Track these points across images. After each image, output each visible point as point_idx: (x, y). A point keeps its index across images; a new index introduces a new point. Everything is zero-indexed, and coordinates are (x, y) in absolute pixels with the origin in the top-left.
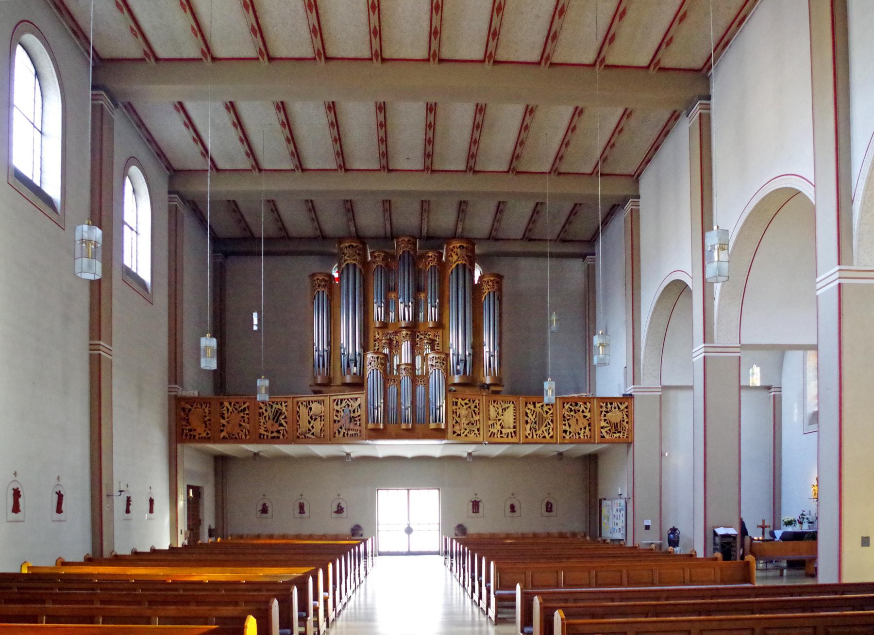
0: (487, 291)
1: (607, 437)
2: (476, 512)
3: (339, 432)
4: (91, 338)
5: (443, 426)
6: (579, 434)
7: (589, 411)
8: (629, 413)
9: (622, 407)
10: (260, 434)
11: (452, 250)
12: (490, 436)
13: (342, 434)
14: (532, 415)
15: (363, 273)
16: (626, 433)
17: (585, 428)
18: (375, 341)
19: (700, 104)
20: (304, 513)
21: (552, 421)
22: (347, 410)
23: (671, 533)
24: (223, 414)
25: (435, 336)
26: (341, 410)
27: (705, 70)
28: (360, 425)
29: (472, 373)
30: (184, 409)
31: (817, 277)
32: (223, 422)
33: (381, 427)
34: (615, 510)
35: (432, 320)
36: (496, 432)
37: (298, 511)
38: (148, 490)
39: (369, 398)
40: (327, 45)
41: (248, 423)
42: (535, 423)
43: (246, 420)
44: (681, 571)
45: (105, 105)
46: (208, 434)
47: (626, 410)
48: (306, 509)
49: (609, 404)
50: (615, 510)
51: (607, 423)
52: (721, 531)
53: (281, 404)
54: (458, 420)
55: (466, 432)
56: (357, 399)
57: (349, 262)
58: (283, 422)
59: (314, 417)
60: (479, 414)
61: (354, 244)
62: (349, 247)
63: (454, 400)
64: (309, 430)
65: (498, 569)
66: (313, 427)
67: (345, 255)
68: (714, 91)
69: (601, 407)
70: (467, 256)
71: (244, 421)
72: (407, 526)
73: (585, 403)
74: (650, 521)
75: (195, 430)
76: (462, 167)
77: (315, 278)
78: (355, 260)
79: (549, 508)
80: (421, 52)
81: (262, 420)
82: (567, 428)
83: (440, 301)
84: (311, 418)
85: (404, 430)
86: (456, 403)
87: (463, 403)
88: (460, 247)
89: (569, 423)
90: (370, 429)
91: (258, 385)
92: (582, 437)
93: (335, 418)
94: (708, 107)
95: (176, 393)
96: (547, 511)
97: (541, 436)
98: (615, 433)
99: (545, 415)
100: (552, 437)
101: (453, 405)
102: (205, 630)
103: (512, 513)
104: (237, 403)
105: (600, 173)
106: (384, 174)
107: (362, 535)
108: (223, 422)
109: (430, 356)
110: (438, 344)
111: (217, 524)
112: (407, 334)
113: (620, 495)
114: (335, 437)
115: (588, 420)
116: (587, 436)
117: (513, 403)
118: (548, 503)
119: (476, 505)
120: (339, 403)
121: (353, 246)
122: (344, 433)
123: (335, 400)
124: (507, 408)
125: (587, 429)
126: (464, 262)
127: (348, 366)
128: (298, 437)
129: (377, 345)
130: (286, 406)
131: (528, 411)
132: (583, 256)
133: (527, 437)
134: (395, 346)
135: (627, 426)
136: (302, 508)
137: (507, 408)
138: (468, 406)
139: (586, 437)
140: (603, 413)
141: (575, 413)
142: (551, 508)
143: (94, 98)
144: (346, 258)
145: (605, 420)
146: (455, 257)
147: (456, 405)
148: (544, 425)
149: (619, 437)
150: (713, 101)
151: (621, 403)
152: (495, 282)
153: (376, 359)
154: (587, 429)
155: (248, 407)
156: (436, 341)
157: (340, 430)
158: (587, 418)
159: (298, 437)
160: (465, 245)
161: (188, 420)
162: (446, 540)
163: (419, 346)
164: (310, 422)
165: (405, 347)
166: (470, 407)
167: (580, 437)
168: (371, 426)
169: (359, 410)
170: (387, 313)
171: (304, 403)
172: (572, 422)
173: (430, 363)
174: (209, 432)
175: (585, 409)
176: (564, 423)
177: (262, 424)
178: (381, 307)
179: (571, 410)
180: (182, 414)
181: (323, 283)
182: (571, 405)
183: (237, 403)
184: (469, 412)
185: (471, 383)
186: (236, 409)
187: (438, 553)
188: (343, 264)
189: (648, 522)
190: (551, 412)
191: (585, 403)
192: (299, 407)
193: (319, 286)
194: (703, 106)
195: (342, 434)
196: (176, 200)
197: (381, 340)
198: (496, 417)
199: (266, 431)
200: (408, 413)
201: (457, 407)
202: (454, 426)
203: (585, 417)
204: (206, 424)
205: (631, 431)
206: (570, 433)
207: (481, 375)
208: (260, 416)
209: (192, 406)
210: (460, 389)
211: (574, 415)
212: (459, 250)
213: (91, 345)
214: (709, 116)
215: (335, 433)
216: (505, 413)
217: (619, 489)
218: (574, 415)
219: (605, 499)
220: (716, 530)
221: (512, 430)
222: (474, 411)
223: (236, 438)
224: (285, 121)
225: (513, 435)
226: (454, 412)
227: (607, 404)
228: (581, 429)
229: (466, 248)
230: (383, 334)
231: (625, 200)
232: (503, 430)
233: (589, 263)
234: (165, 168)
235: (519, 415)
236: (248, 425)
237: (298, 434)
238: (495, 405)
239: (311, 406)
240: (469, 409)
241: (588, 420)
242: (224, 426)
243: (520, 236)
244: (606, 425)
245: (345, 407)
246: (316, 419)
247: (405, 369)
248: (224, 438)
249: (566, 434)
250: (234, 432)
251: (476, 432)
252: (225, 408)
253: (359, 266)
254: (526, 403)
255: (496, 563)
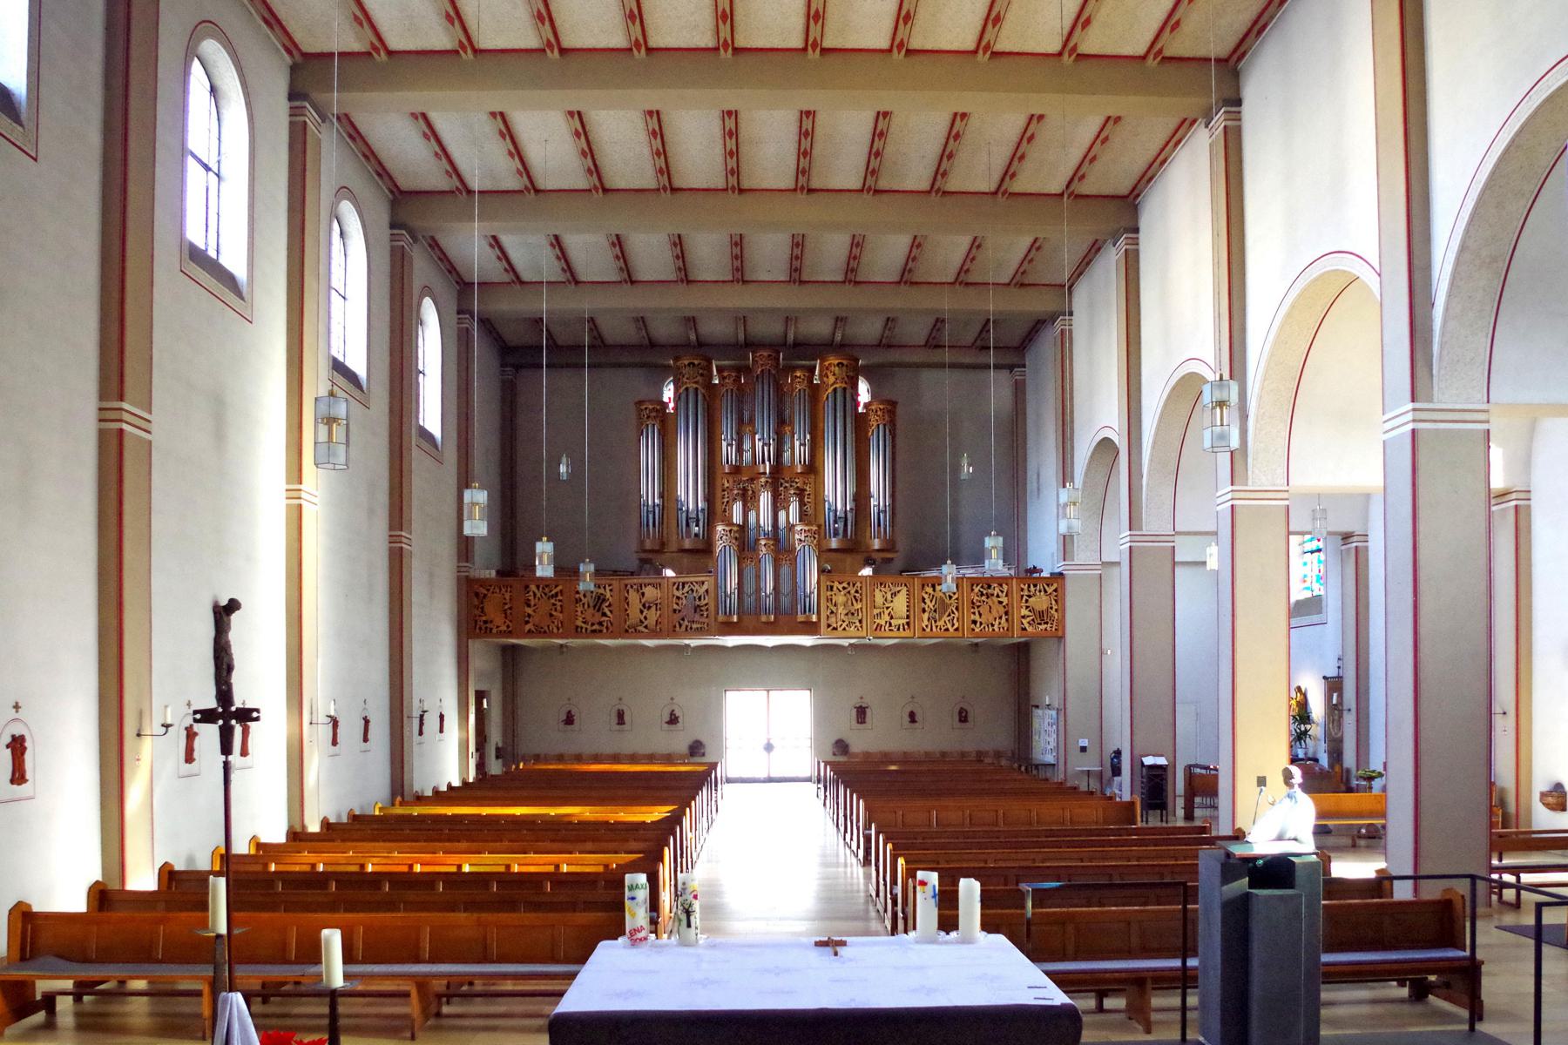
0: (875, 424)
1: (1030, 629)
2: (861, 723)
3: (680, 625)
4: (391, 529)
5: (814, 618)
6: (993, 625)
7: (1007, 596)
8: (1059, 597)
9: (1050, 590)
10: (577, 627)
11: (827, 369)
12: (876, 630)
13: (684, 627)
14: (931, 601)
15: (707, 398)
16: (1055, 623)
17: (1000, 618)
18: (724, 491)
19: (1126, 238)
20: (624, 724)
21: (957, 609)
22: (691, 596)
23: (1115, 757)
24: (529, 600)
25: (804, 483)
26: (683, 597)
27: (1132, 197)
28: (707, 617)
29: (855, 534)
30: (477, 595)
31: (1217, 491)
32: (529, 610)
33: (735, 619)
34: (1046, 724)
35: (800, 462)
36: (883, 623)
37: (616, 721)
38: (438, 703)
39: (719, 581)
40: (650, 32)
41: (561, 612)
42: (935, 611)
43: (559, 608)
44: (1061, 812)
45: (406, 246)
46: (508, 627)
47: (1055, 594)
48: (627, 718)
49: (1032, 586)
50: (1046, 724)
51: (1030, 611)
52: (1148, 761)
53: (605, 588)
54: (834, 609)
55: (844, 625)
56: (703, 583)
57: (688, 385)
58: (606, 610)
59: (647, 605)
60: (861, 600)
61: (696, 362)
62: (689, 364)
63: (828, 583)
64: (641, 622)
65: (866, 808)
66: (646, 618)
67: (683, 376)
68: (1144, 224)
69: (1022, 590)
70: (848, 376)
71: (556, 610)
72: (766, 742)
73: (1001, 585)
74: (1087, 740)
75: (491, 622)
76: (840, 278)
77: (643, 407)
78: (696, 383)
79: (963, 717)
80: (787, 182)
81: (579, 609)
82: (977, 617)
83: (811, 438)
84: (644, 606)
85: (764, 623)
86: (832, 587)
87: (840, 587)
88: (838, 364)
89: (979, 612)
90: (722, 623)
91: (581, 570)
92: (997, 629)
93: (675, 607)
94: (1136, 242)
95: (467, 574)
96: (960, 721)
97: (943, 628)
98: (1040, 624)
99: (947, 601)
100: (957, 629)
101: (827, 590)
102: (627, 860)
103: (912, 725)
104: (547, 586)
105: (1020, 282)
106: (738, 287)
107: (703, 755)
108: (529, 610)
109: (798, 528)
110: (809, 495)
111: (503, 742)
112: (767, 482)
113: (1048, 705)
114: (674, 631)
115: (1004, 607)
116: (1003, 628)
117: (906, 585)
118: (962, 711)
119: (861, 713)
120: (681, 587)
121: (694, 364)
122: (687, 626)
123: (674, 584)
124: (899, 592)
125: (1004, 618)
126: (844, 385)
127: (688, 525)
128: (627, 631)
129: (726, 496)
130: (611, 590)
131: (926, 596)
132: (1011, 367)
133: (924, 630)
134: (751, 498)
135: (1056, 615)
136: (621, 717)
137: (899, 592)
138: (846, 591)
139: (1001, 630)
140: (1025, 597)
141: (987, 598)
142: (966, 717)
143: (393, 238)
144: (685, 380)
145: (1027, 607)
146: (832, 379)
147: (832, 590)
148: (947, 614)
149: (1046, 630)
150: (1142, 235)
151: (1048, 585)
152: (885, 411)
153: (728, 533)
154: (1004, 618)
155: (561, 591)
156: (806, 490)
157: (682, 622)
158: (1004, 604)
159: (627, 631)
160: (845, 362)
161: (482, 608)
162: (819, 763)
163: (782, 497)
164: (642, 612)
165: (765, 499)
166: (849, 592)
167: (993, 630)
168: (721, 618)
169: (706, 597)
170: (740, 450)
171: (635, 587)
172: (984, 609)
173: (797, 537)
174: (510, 624)
175: (1000, 594)
176: (972, 610)
177: (579, 613)
178: (732, 445)
179: (982, 594)
180: (476, 602)
181: (654, 414)
182: (982, 587)
183: (547, 586)
184: (848, 600)
185: (854, 548)
186: (546, 594)
187: (809, 780)
188: (680, 387)
189: (1084, 742)
190: (956, 596)
191: (1001, 585)
192: (628, 592)
193: (648, 417)
194: (1130, 241)
195: (684, 627)
196: (467, 321)
197: (731, 490)
198: (884, 604)
199: (584, 623)
200: (770, 601)
201: (833, 593)
202: (828, 617)
203: (1001, 603)
204: (506, 614)
205: (1062, 623)
206: (981, 624)
207: (868, 537)
208: (577, 603)
209: (488, 590)
210: (839, 556)
211: (986, 600)
212: (837, 368)
213: (390, 536)
214: (1137, 252)
215: (675, 627)
216: (895, 599)
217: (1047, 698)
218: (986, 600)
219: (1037, 707)
220: (1144, 759)
221: (905, 621)
222: (855, 597)
223: (545, 632)
224: (586, 149)
225: (906, 627)
226: (829, 600)
227: (1029, 586)
228: (995, 619)
229: (847, 366)
230: (734, 482)
231: (1053, 318)
232: (892, 621)
233: (1017, 377)
234: (454, 283)
235: (914, 599)
236: (561, 615)
237: (626, 627)
238: (883, 589)
239: (644, 590)
240: (848, 595)
241: (1004, 607)
242: (529, 616)
243: (923, 343)
244: (1027, 613)
245: (687, 592)
246: (649, 608)
247: (765, 545)
248: (529, 631)
249: (976, 625)
250: (542, 625)
251: (858, 624)
252: (531, 593)
253: (701, 391)
254: (923, 586)
255: (865, 801)
